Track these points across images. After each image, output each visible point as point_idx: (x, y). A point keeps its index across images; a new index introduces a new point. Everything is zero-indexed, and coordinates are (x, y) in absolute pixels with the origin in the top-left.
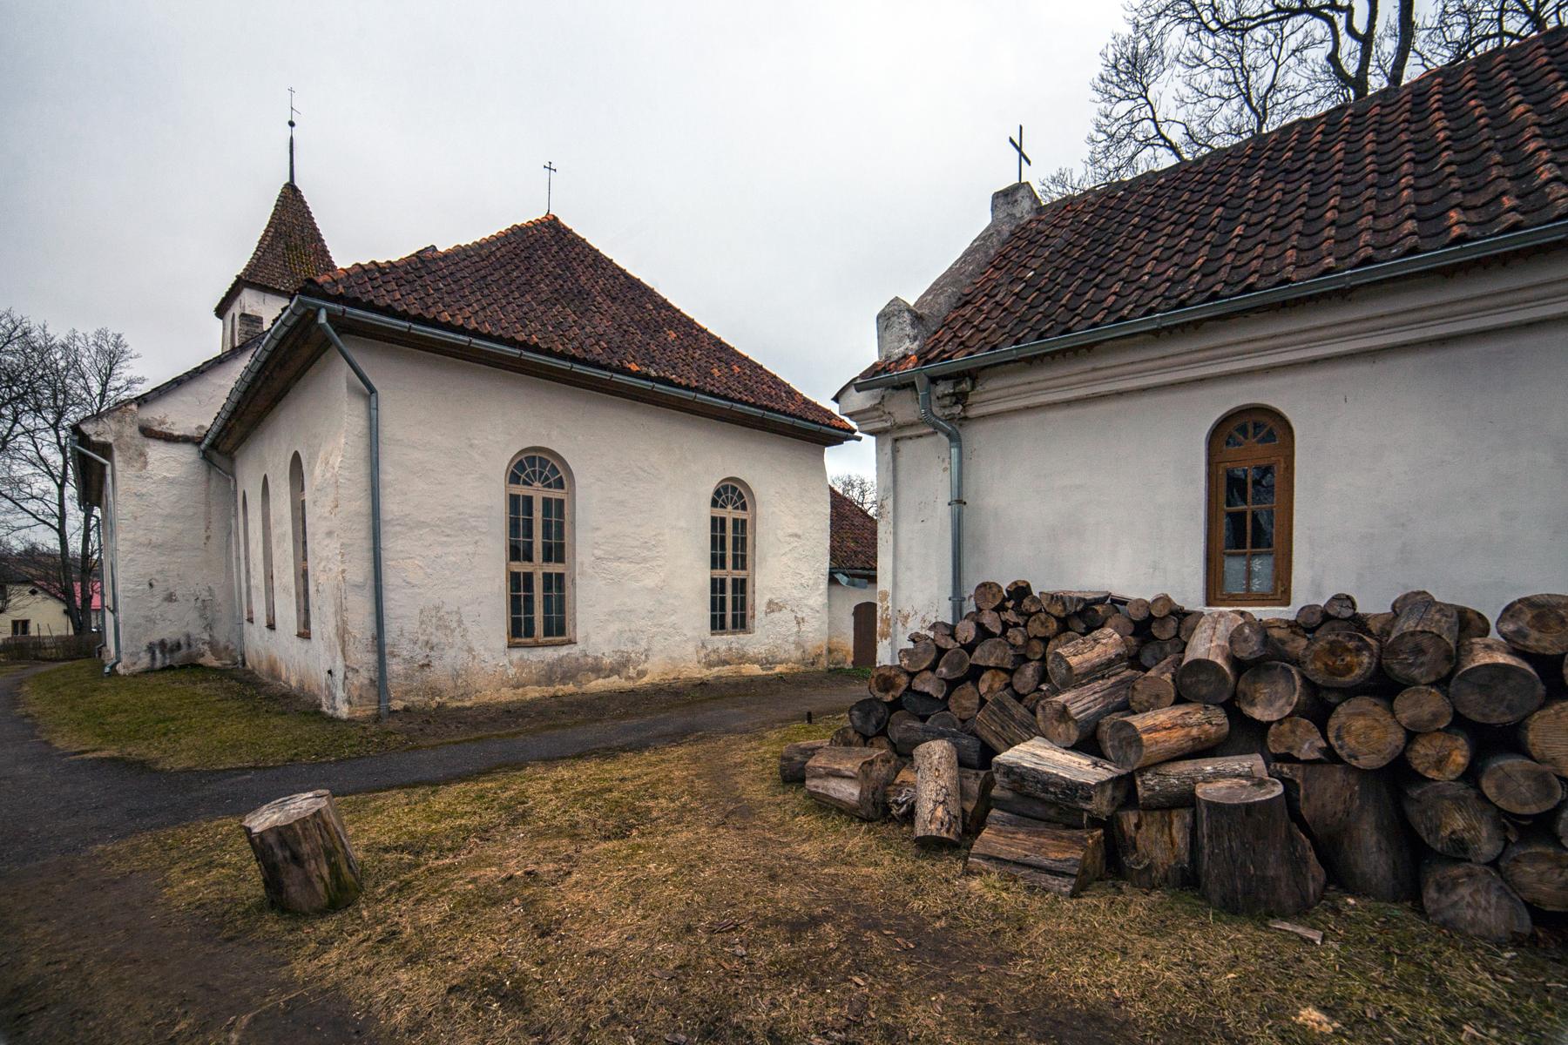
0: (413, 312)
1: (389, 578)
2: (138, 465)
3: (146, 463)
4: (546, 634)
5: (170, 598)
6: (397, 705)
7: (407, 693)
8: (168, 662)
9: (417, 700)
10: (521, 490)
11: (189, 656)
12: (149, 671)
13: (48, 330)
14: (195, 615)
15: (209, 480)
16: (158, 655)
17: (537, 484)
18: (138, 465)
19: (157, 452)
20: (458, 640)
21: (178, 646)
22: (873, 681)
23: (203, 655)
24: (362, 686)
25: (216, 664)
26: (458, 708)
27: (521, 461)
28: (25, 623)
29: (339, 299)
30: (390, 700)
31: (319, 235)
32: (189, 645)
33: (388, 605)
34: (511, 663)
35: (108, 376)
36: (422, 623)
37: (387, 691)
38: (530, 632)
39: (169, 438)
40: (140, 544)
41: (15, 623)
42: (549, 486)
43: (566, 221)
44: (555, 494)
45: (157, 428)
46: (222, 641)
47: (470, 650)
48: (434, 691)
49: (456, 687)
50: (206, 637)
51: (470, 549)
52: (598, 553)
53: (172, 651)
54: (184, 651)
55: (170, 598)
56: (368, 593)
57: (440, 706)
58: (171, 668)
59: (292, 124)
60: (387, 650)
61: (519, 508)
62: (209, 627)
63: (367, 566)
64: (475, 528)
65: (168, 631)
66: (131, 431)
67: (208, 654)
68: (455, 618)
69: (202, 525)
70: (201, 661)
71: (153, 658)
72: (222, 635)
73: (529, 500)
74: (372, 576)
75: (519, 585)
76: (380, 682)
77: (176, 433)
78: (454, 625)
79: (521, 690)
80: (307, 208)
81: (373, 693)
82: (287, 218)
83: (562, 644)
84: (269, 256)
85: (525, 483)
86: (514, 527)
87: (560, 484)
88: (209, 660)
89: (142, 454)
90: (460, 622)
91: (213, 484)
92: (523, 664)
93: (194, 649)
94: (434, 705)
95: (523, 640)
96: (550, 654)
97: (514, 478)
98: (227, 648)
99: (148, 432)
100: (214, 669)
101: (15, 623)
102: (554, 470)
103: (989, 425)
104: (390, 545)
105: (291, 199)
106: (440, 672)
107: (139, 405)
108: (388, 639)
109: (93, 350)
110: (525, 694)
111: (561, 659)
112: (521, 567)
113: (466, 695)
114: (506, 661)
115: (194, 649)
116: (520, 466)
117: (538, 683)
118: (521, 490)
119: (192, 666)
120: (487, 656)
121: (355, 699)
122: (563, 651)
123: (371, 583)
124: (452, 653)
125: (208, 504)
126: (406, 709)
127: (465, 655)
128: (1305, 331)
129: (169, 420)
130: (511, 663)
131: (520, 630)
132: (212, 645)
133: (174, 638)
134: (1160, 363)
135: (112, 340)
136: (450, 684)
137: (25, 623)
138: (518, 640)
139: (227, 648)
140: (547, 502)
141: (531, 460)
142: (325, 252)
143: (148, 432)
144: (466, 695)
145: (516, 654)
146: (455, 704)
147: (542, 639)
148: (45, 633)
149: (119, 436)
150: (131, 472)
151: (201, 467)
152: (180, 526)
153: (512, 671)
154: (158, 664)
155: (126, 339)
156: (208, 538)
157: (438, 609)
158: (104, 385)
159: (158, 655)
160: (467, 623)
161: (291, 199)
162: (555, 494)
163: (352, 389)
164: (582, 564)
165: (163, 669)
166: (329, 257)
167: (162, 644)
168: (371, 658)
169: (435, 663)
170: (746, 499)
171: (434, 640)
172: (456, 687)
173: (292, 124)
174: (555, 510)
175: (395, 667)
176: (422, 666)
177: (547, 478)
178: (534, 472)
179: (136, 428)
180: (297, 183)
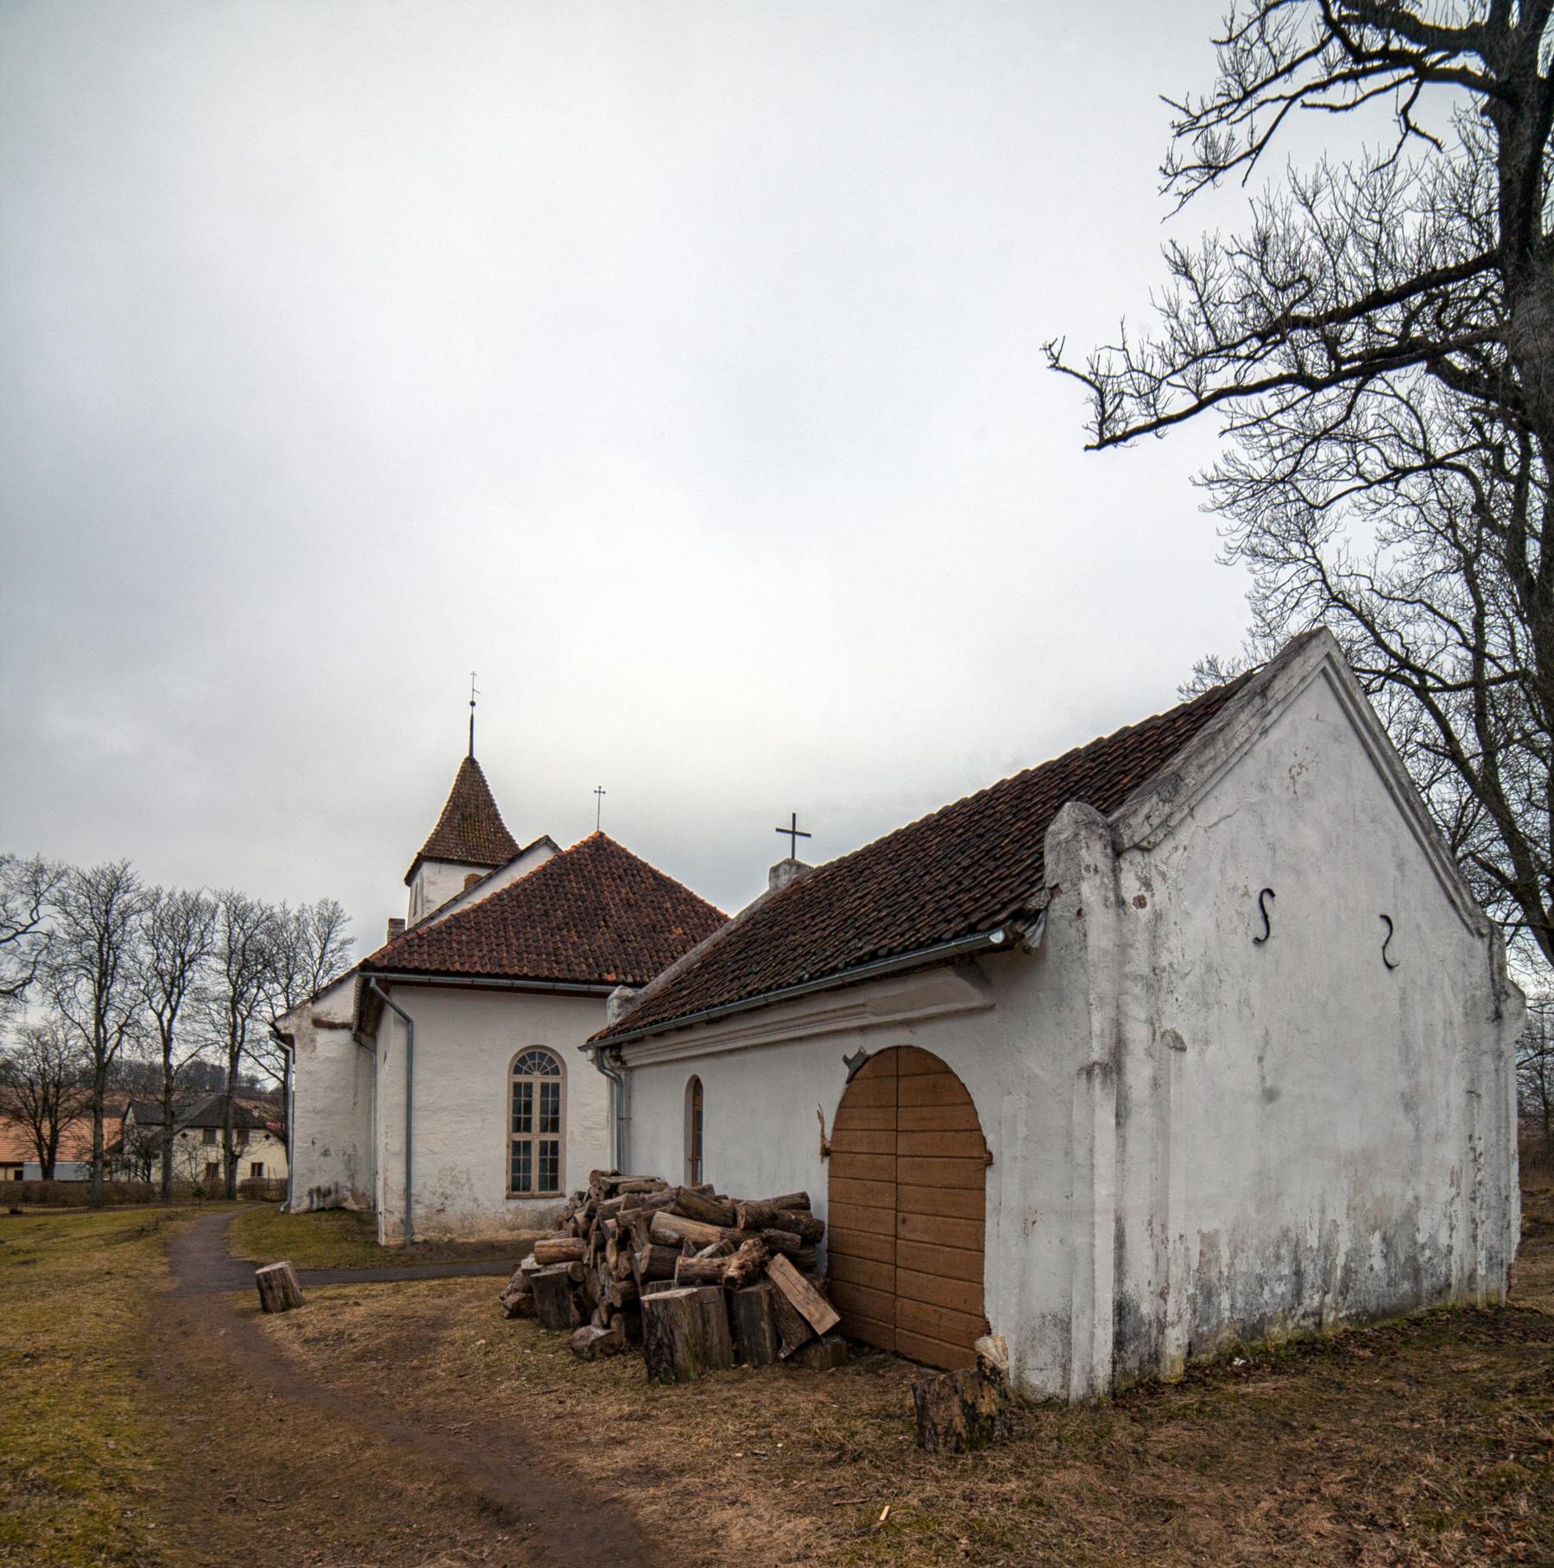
0: (433, 968)
1: (417, 1147)
2: (309, 1049)
3: (315, 1047)
4: (541, 1189)
5: (326, 1153)
6: (419, 1238)
7: (426, 1230)
8: (321, 1204)
9: (434, 1235)
10: (522, 1079)
11: (337, 1201)
12: (309, 1211)
13: (287, 906)
14: (341, 1166)
15: (357, 1058)
16: (315, 1199)
17: (536, 1073)
18: (309, 1049)
19: (323, 1037)
20: (466, 1191)
21: (329, 1192)
22: (1251, 1253)
23: (346, 1200)
24: (394, 1224)
25: (355, 1207)
26: (464, 1243)
27: (523, 1057)
28: (260, 1165)
29: (382, 969)
30: (413, 1234)
31: (492, 800)
32: (337, 1191)
33: (414, 1167)
34: (508, 1211)
35: (327, 940)
36: (440, 1179)
37: (412, 1227)
38: (527, 1188)
39: (332, 1026)
40: (309, 1111)
41: (253, 1165)
42: (547, 1073)
43: (610, 835)
44: (551, 1079)
45: (324, 1019)
46: (361, 1188)
47: (475, 1200)
48: (447, 1230)
49: (463, 1227)
50: (349, 1185)
51: (479, 1125)
52: (587, 1124)
53: (325, 1196)
54: (333, 1196)
55: (326, 1153)
56: (403, 1158)
57: (451, 1241)
58: (322, 1210)
59: (473, 704)
60: (413, 1199)
61: (520, 1093)
62: (352, 1177)
63: (403, 1139)
64: (482, 1109)
65: (322, 1181)
66: (307, 1023)
67: (350, 1199)
68: (465, 1176)
69: (351, 1092)
70: (345, 1205)
71: (312, 1202)
72: (361, 1184)
73: (529, 1086)
74: (404, 1146)
75: (519, 1150)
76: (407, 1222)
77: (337, 1021)
78: (463, 1181)
79: (516, 1232)
80: (482, 777)
81: (402, 1229)
82: (464, 791)
83: (554, 1197)
84: (447, 829)
85: (526, 1073)
86: (516, 1108)
87: (556, 1071)
88: (351, 1204)
89: (313, 1041)
90: (469, 1179)
91: (361, 1059)
92: (518, 1212)
93: (340, 1195)
94: (446, 1239)
95: (521, 1193)
96: (542, 1205)
97: (517, 1070)
98: (364, 1195)
99: (318, 1023)
100: (353, 1212)
101: (253, 1165)
102: (551, 1061)
103: (646, 1072)
104: (420, 1126)
105: (471, 764)
106: (452, 1215)
107: (313, 1003)
108: (414, 1191)
109: (316, 918)
110: (519, 1236)
111: (551, 1210)
112: (521, 1137)
113: (471, 1233)
114: (504, 1209)
115: (340, 1195)
116: (523, 1060)
117: (531, 1227)
118: (522, 1079)
119: (338, 1209)
120: (488, 1204)
121: (390, 1233)
122: (554, 1203)
123: (404, 1151)
124: (461, 1202)
125: (356, 1076)
126: (425, 1242)
127: (472, 1203)
128: (812, 1015)
129: (333, 1012)
130: (508, 1211)
131: (518, 1186)
132: (353, 1191)
133: (327, 1185)
134: (761, 1030)
135: (331, 907)
136: (459, 1225)
137: (260, 1165)
138: (516, 1193)
139: (364, 1195)
140: (544, 1087)
141: (532, 1055)
142: (496, 815)
143: (318, 1023)
144: (471, 1233)
145: (513, 1204)
146: (461, 1240)
147: (537, 1193)
148: (273, 1177)
149: (299, 1028)
150: (305, 1054)
151: (353, 1045)
152: (336, 1096)
153: (508, 1217)
154: (315, 1207)
155: (341, 905)
156: (355, 1104)
157: (452, 1169)
158: (323, 949)
159: (315, 1199)
160: (474, 1180)
161: (471, 764)
162: (551, 1079)
163: (396, 1021)
164: (572, 1133)
165: (318, 1210)
166: (500, 820)
167: (319, 1190)
168: (402, 1204)
169: (448, 1209)
170: (558, 1063)
171: (448, 1192)
172: (463, 1227)
173: (473, 704)
174: (552, 1093)
175: (419, 1211)
176: (439, 1211)
177: (545, 1067)
178: (534, 1064)
179: (310, 1021)
180: (475, 756)
